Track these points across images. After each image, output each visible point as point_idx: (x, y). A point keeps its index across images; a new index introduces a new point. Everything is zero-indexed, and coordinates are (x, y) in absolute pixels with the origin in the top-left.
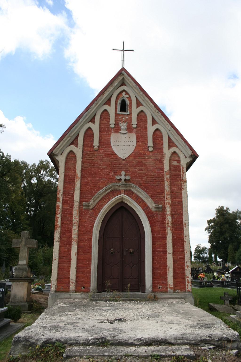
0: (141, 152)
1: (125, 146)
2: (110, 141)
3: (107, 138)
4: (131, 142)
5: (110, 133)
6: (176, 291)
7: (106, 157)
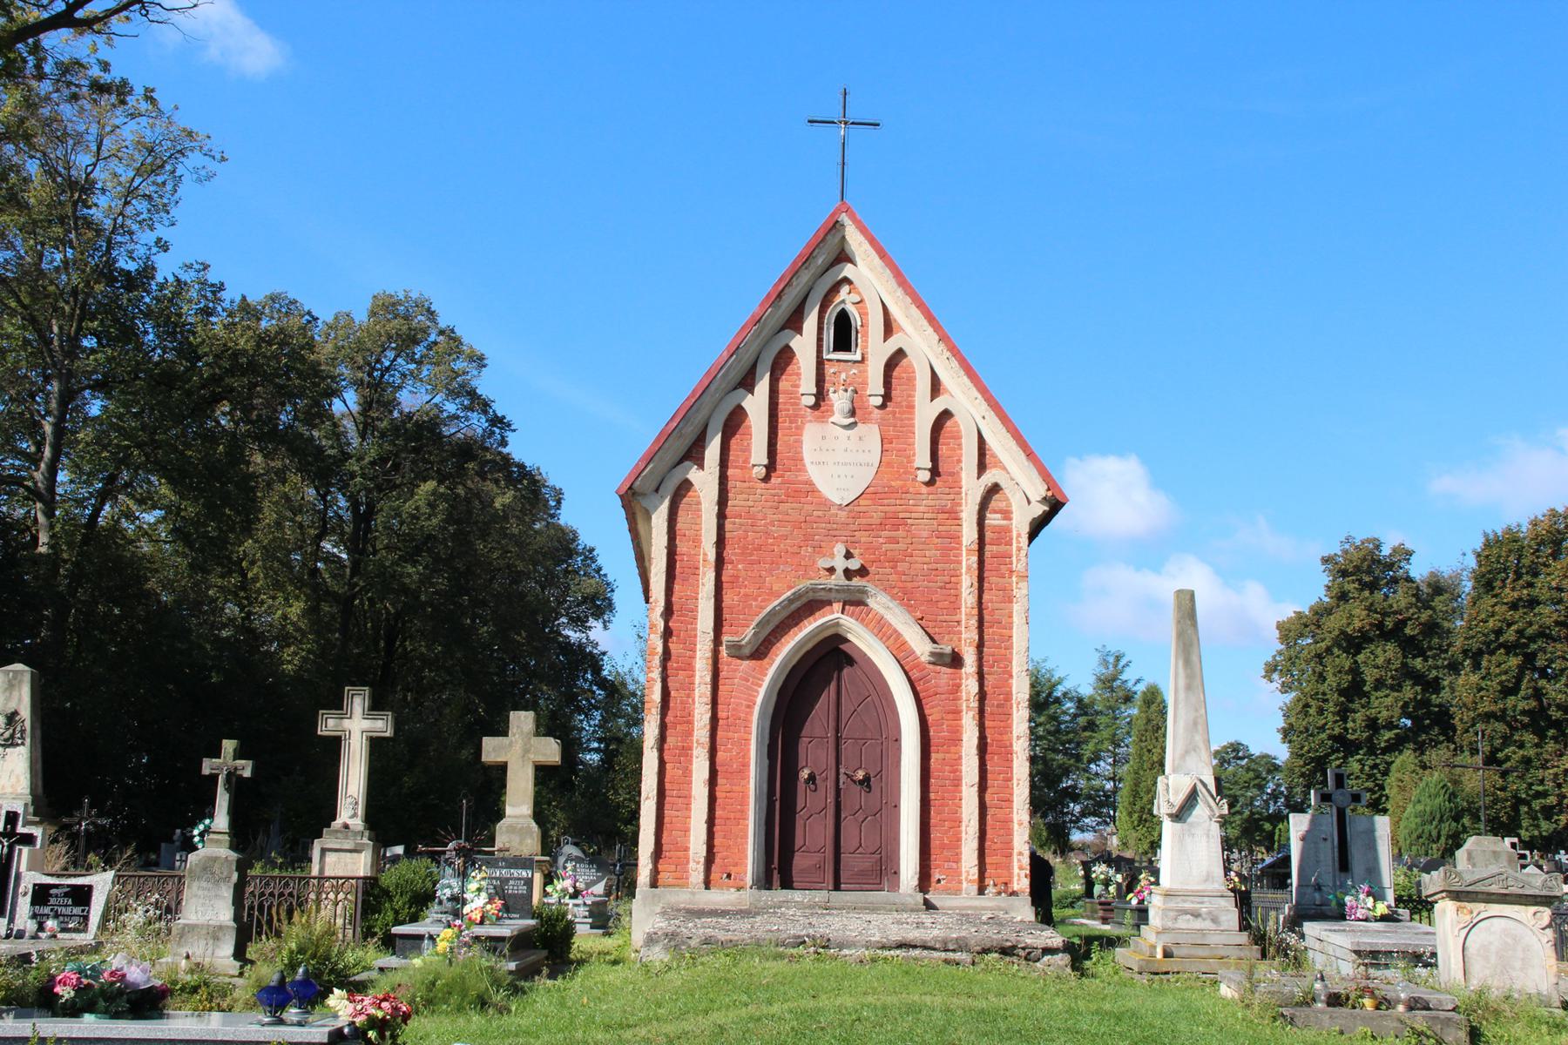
0: (893, 483)
1: (846, 464)
3: (792, 438)
7: (790, 499)
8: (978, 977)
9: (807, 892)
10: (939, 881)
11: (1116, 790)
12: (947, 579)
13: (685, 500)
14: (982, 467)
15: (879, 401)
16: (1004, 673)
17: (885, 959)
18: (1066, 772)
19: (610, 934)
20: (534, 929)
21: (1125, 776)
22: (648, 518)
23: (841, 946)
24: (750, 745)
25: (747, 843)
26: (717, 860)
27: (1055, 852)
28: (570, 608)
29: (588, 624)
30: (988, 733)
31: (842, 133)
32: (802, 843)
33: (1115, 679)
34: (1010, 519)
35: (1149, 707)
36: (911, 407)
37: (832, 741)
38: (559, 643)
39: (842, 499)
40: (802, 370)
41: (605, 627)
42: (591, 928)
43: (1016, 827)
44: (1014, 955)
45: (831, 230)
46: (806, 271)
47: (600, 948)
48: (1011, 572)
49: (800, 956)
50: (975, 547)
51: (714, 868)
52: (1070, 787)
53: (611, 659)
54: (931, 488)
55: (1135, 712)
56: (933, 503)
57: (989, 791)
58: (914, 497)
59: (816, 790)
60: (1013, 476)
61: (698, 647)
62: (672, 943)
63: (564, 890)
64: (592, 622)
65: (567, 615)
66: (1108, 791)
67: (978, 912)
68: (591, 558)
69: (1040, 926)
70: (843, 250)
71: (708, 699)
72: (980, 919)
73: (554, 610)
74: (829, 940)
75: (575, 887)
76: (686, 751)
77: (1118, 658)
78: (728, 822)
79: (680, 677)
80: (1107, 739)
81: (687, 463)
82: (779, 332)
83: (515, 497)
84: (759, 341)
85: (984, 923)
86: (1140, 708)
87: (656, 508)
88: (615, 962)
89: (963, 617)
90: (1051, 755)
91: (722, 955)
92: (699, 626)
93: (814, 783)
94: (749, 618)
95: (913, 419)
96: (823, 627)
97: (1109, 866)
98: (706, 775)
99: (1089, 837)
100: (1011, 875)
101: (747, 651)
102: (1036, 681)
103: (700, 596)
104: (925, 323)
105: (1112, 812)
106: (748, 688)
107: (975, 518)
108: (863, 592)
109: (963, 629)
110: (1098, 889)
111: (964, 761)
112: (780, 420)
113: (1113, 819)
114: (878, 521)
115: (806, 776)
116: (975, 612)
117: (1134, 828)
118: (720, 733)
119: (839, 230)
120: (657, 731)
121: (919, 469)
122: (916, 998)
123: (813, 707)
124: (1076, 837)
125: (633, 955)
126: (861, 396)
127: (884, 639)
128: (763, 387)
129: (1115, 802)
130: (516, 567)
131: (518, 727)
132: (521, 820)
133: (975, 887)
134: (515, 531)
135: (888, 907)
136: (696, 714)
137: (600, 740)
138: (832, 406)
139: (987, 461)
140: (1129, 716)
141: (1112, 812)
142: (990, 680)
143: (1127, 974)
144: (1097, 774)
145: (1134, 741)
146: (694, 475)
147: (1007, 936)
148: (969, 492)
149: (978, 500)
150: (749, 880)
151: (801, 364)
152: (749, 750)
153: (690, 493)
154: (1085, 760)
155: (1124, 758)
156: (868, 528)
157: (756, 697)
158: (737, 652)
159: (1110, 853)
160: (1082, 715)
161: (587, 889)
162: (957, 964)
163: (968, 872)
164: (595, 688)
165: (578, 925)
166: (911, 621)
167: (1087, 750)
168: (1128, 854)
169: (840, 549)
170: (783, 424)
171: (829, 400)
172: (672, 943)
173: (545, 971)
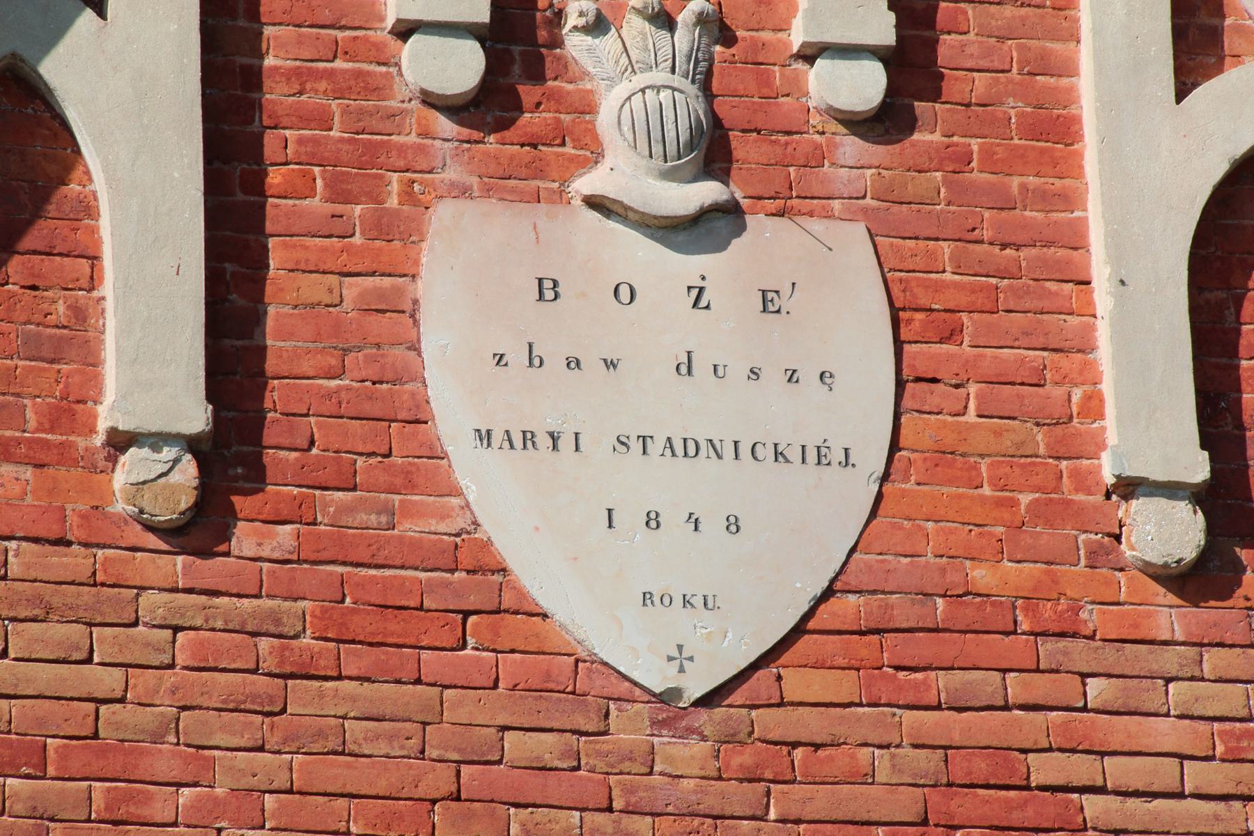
0: (981, 575)
1: (690, 449)
2: (415, 348)
3: (353, 288)
4: (792, 376)
5: (408, 195)
6: (723, 704)
7: (355, 659)
54: (1210, 616)
58: (1110, 657)
112: (275, 177)
138: (587, 107)
171: (565, 68)
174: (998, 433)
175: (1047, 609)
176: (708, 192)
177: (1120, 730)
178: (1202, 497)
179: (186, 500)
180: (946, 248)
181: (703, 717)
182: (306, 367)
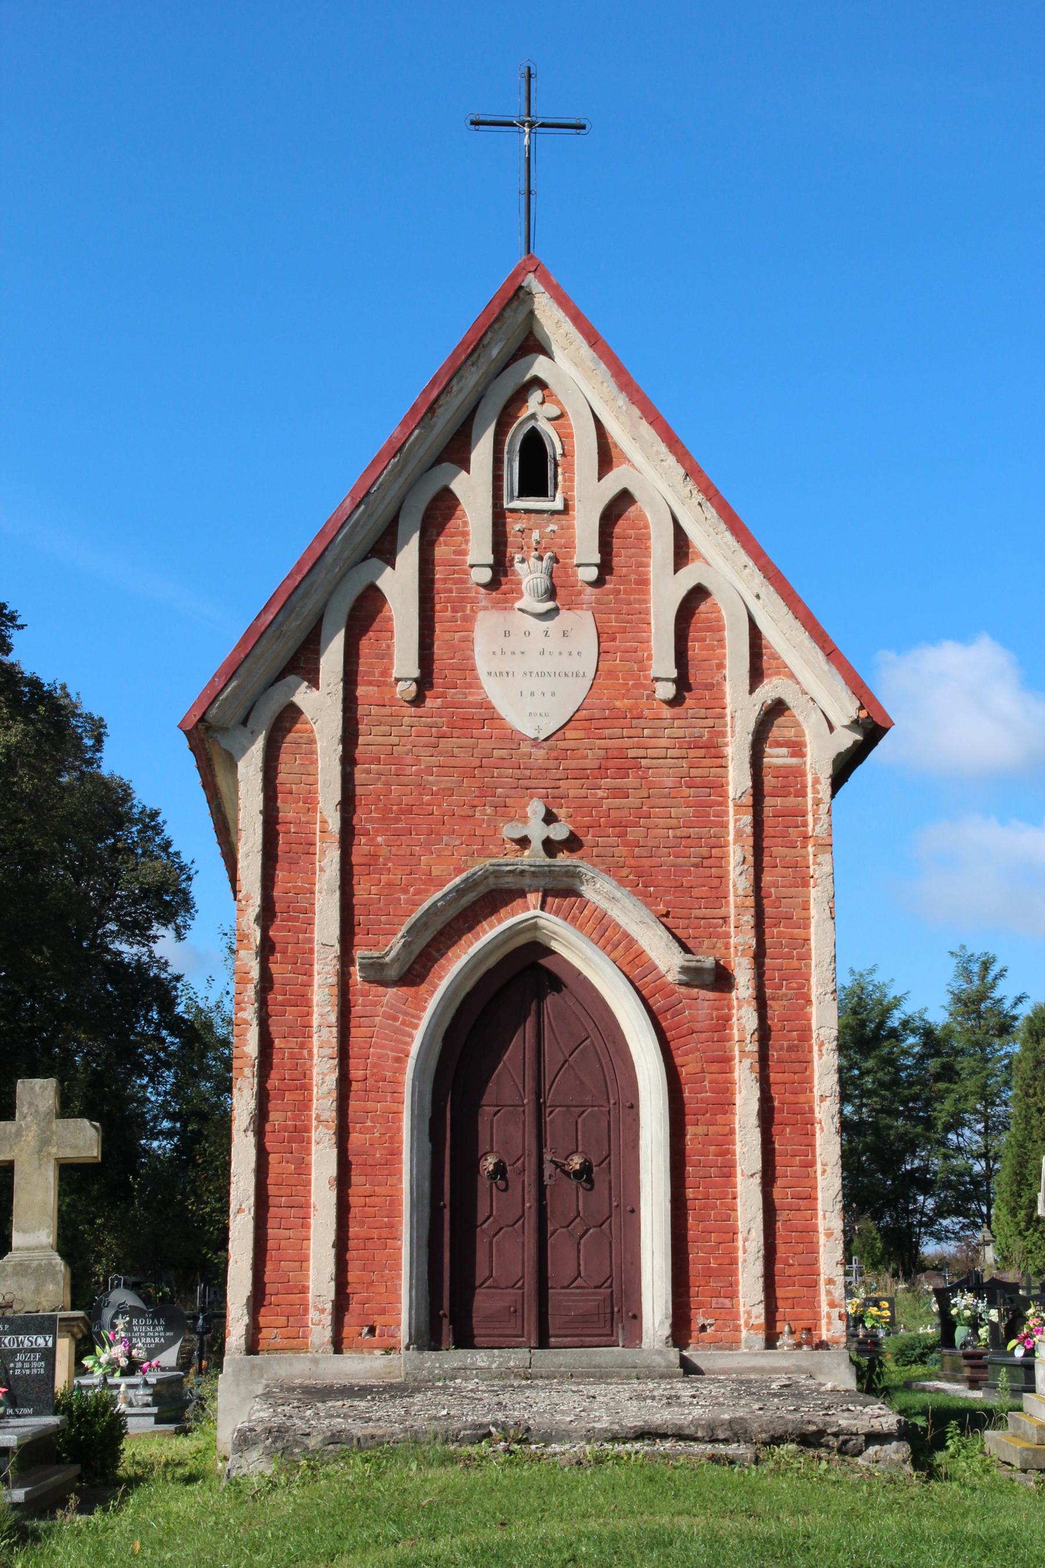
0: (618, 704)
1: (542, 674)
2: (473, 650)
3: (457, 635)
4: (570, 654)
5: (472, 610)
7: (456, 732)
8: (765, 1483)
9: (496, 1351)
10: (703, 1328)
11: (989, 1174)
12: (704, 851)
13: (291, 737)
14: (756, 675)
15: (592, 574)
16: (798, 997)
17: (618, 1457)
18: (911, 1146)
19: (184, 1431)
20: (58, 1430)
21: (1004, 1152)
22: (233, 767)
23: (547, 1439)
24: (400, 1120)
25: (399, 1276)
26: (354, 1306)
27: (895, 1275)
28: (121, 906)
29: (152, 933)
30: (775, 1091)
31: (526, 142)
32: (487, 1274)
33: (982, 997)
34: (802, 755)
35: (1038, 1042)
36: (643, 582)
37: (530, 1110)
38: (106, 965)
39: (538, 729)
40: (470, 528)
41: (180, 937)
42: (157, 1422)
43: (822, 1239)
44: (821, 1445)
45: (511, 300)
46: (473, 369)
47: (170, 1455)
48: (806, 838)
49: (483, 1458)
50: (748, 800)
51: (348, 1319)
52: (918, 1169)
53: (187, 987)
54: (677, 710)
55: (1017, 1049)
56: (680, 733)
57: (779, 1182)
58: (650, 723)
59: (506, 1190)
60: (805, 686)
61: (316, 967)
62: (279, 1445)
63: (113, 1363)
64: (157, 929)
65: (117, 919)
66: (978, 1175)
67: (766, 1377)
68: (154, 828)
69: (862, 1397)
70: (531, 333)
71: (332, 1050)
72: (768, 1387)
73: (95, 911)
74: (528, 1429)
75: (129, 1357)
76: (300, 1134)
77: (986, 966)
78: (369, 1244)
79: (288, 1017)
80: (973, 1094)
81: (291, 679)
82: (432, 466)
83: (25, 734)
84: (401, 481)
85: (775, 1395)
86: (1024, 1043)
87: (244, 750)
88: (190, 1479)
89: (732, 911)
90: (885, 1120)
91: (358, 1459)
92: (316, 936)
93: (504, 1178)
94: (396, 920)
95: (646, 601)
96: (513, 932)
97: (978, 1296)
98: (332, 1170)
99: (949, 1248)
100: (816, 1316)
101: (393, 973)
102: (859, 1004)
103: (317, 887)
104: (663, 448)
105: (984, 1209)
106: (397, 1031)
107: (746, 755)
108: (573, 874)
109: (732, 929)
110: (961, 1333)
111: (738, 1137)
112: (438, 607)
113: (987, 1219)
114: (595, 764)
115: (491, 1168)
116: (750, 902)
117: (1020, 1233)
118: (353, 1104)
119: (523, 302)
120: (253, 1104)
121: (657, 679)
122: (665, 1520)
123: (499, 1058)
124: (930, 1248)
125: (220, 1465)
126: (565, 567)
127: (609, 947)
128: (409, 555)
129: (988, 1192)
130: (32, 845)
131: (31, 1104)
132: (36, 1254)
133: (761, 1336)
134: (27, 786)
135: (625, 1372)
136: (315, 1075)
137: (173, 1117)
138: (519, 583)
139: (765, 665)
140: (1007, 1055)
141: (984, 1209)
142: (776, 1009)
143: (1002, 1473)
144: (959, 1149)
145: (1016, 1095)
146: (304, 697)
147: (811, 1416)
148: (737, 715)
149: (751, 726)
150: (403, 1335)
151: (469, 518)
152: (399, 1129)
153: (298, 726)
154: (940, 1126)
155: (1001, 1123)
156: (580, 774)
157: (409, 1044)
158: (377, 974)
159: (978, 1276)
160: (932, 1056)
161: (149, 1360)
162: (732, 1462)
163: (749, 1313)
164: (164, 1033)
165: (129, 1419)
166: (650, 919)
167: (943, 1110)
168: (1011, 1276)
169: (536, 809)
170: (442, 614)
171: (514, 573)
172: (279, 1445)
173: (73, 1500)
174: (624, 666)
175: (635, 712)
176: (550, 605)
177: (652, 742)
178: (674, 681)
179: (413, 695)
180: (613, 616)
181: (544, 743)
182: (445, 657)
